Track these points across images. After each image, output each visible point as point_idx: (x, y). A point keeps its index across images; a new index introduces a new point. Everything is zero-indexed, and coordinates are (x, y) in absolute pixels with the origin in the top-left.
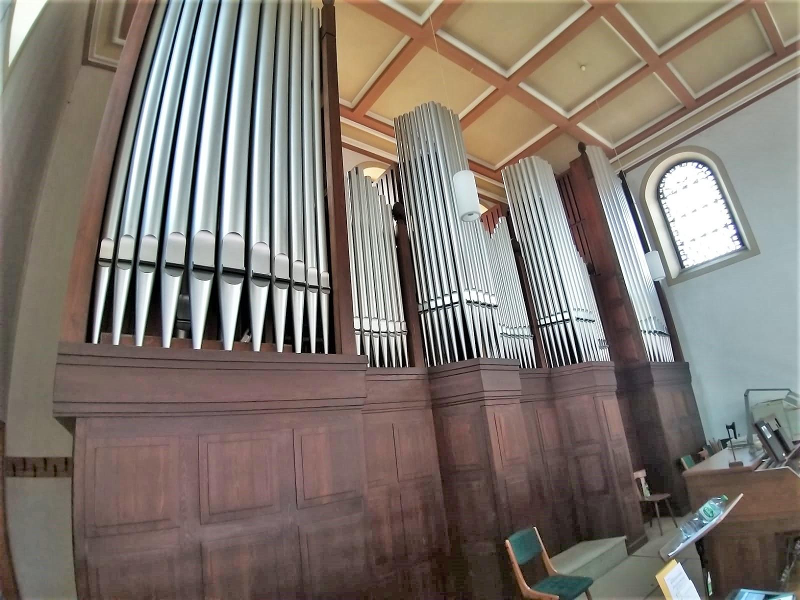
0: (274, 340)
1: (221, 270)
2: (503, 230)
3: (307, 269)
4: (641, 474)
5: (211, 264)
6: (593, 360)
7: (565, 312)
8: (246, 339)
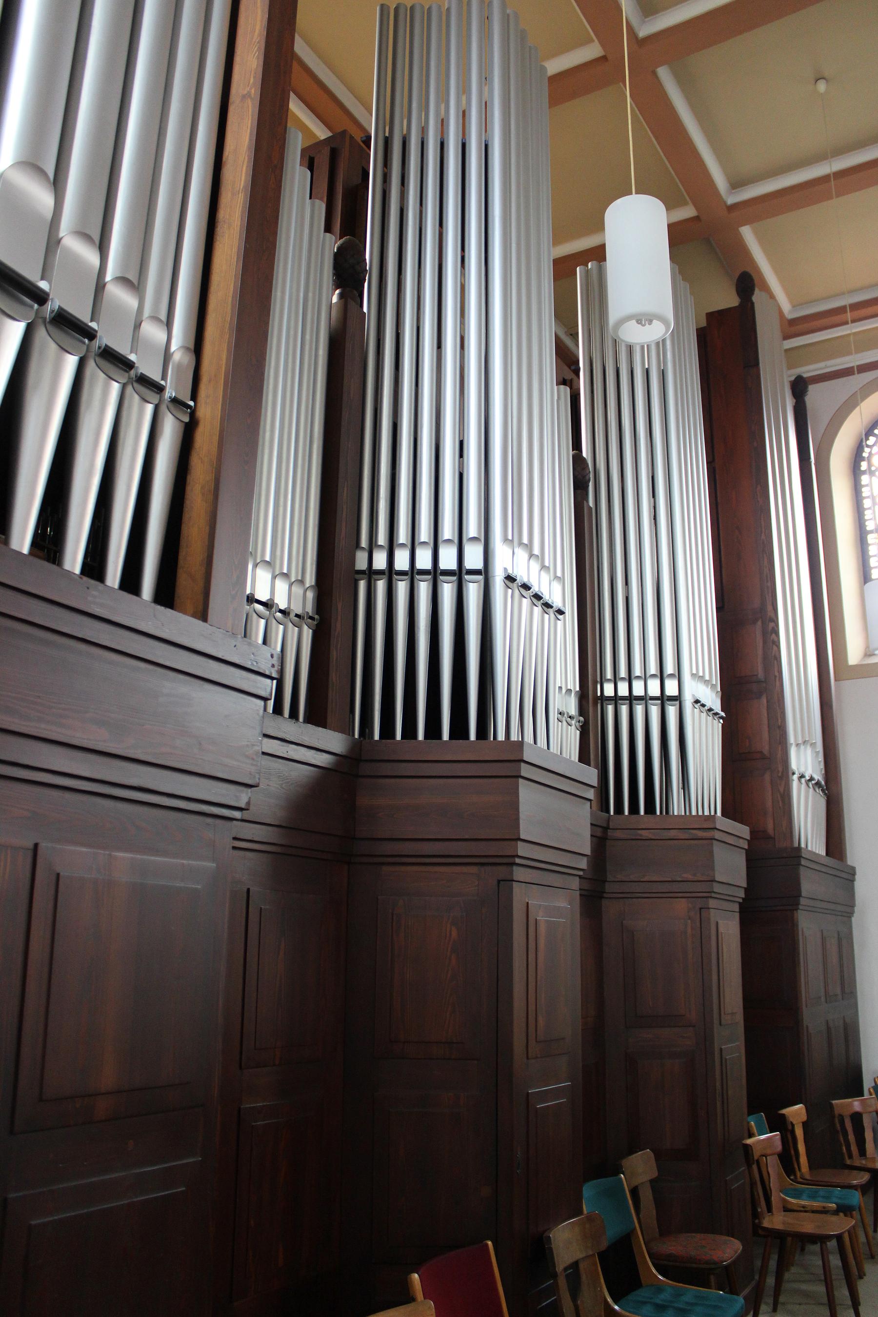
7: (623, 679)
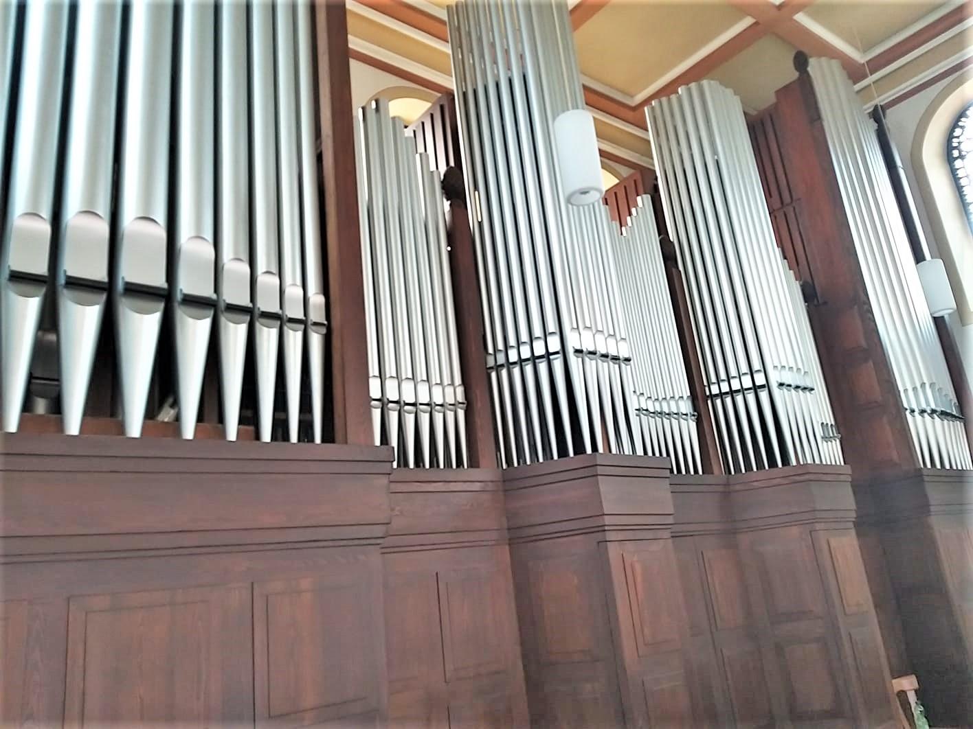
0: (221, 419)
1: (120, 286)
2: (644, 214)
3: (220, 266)
4: (908, 684)
5: (101, 275)
6: (809, 462)
7: (758, 371)
8: (166, 415)
